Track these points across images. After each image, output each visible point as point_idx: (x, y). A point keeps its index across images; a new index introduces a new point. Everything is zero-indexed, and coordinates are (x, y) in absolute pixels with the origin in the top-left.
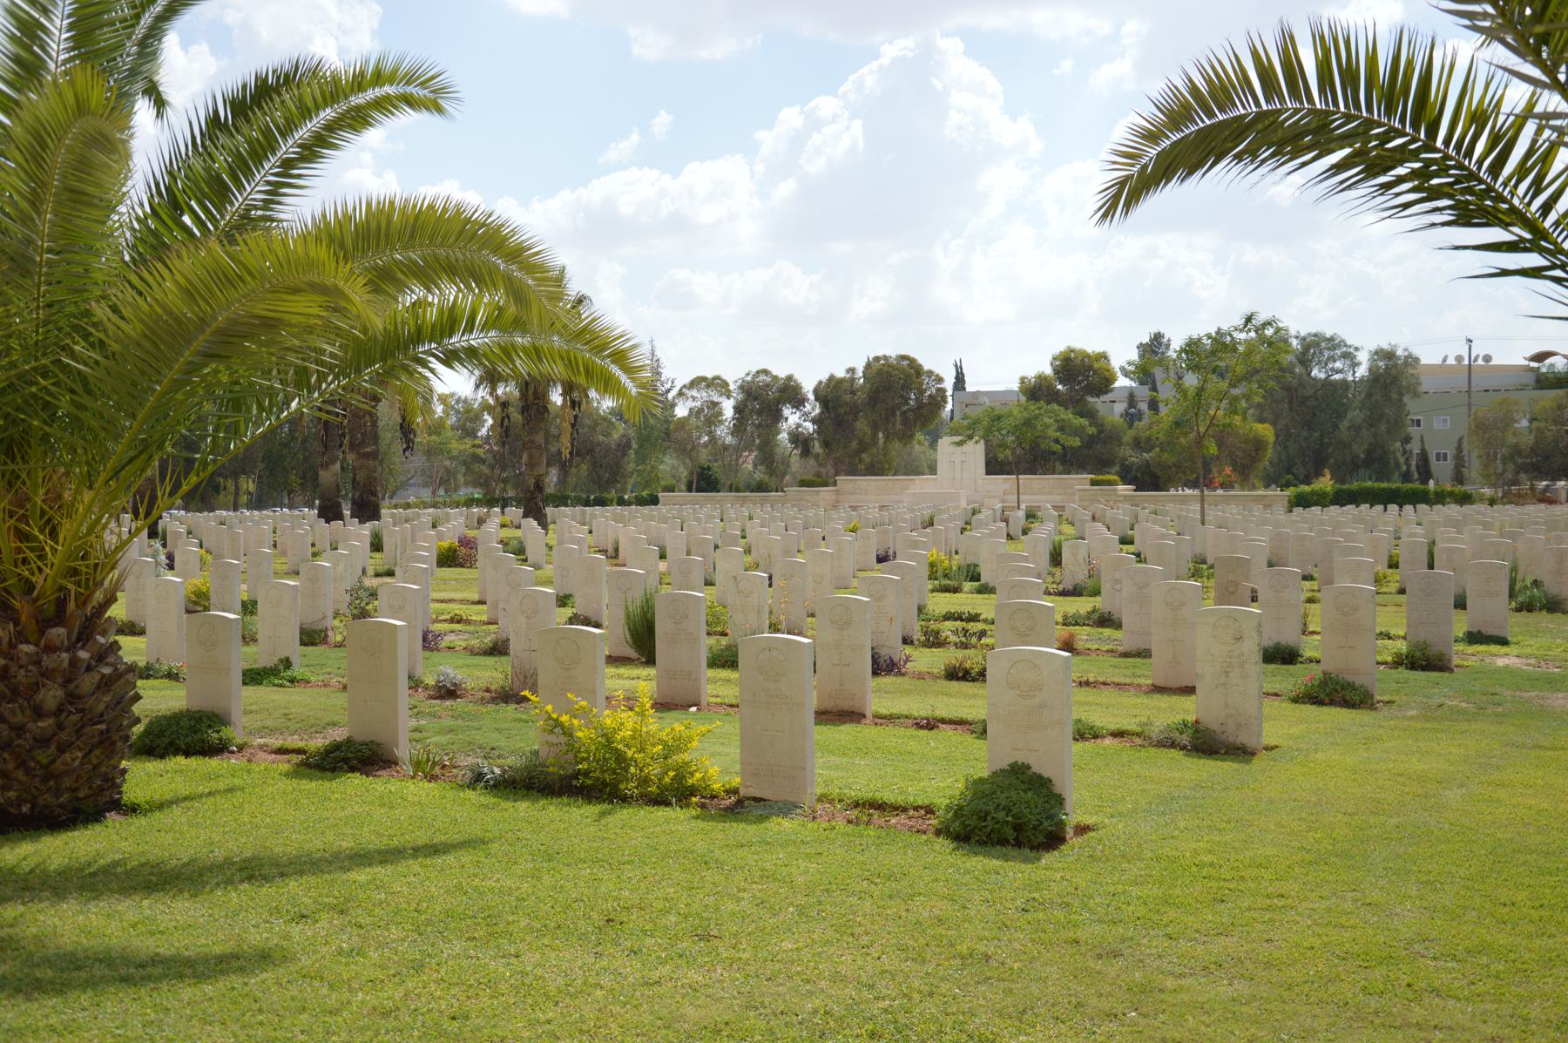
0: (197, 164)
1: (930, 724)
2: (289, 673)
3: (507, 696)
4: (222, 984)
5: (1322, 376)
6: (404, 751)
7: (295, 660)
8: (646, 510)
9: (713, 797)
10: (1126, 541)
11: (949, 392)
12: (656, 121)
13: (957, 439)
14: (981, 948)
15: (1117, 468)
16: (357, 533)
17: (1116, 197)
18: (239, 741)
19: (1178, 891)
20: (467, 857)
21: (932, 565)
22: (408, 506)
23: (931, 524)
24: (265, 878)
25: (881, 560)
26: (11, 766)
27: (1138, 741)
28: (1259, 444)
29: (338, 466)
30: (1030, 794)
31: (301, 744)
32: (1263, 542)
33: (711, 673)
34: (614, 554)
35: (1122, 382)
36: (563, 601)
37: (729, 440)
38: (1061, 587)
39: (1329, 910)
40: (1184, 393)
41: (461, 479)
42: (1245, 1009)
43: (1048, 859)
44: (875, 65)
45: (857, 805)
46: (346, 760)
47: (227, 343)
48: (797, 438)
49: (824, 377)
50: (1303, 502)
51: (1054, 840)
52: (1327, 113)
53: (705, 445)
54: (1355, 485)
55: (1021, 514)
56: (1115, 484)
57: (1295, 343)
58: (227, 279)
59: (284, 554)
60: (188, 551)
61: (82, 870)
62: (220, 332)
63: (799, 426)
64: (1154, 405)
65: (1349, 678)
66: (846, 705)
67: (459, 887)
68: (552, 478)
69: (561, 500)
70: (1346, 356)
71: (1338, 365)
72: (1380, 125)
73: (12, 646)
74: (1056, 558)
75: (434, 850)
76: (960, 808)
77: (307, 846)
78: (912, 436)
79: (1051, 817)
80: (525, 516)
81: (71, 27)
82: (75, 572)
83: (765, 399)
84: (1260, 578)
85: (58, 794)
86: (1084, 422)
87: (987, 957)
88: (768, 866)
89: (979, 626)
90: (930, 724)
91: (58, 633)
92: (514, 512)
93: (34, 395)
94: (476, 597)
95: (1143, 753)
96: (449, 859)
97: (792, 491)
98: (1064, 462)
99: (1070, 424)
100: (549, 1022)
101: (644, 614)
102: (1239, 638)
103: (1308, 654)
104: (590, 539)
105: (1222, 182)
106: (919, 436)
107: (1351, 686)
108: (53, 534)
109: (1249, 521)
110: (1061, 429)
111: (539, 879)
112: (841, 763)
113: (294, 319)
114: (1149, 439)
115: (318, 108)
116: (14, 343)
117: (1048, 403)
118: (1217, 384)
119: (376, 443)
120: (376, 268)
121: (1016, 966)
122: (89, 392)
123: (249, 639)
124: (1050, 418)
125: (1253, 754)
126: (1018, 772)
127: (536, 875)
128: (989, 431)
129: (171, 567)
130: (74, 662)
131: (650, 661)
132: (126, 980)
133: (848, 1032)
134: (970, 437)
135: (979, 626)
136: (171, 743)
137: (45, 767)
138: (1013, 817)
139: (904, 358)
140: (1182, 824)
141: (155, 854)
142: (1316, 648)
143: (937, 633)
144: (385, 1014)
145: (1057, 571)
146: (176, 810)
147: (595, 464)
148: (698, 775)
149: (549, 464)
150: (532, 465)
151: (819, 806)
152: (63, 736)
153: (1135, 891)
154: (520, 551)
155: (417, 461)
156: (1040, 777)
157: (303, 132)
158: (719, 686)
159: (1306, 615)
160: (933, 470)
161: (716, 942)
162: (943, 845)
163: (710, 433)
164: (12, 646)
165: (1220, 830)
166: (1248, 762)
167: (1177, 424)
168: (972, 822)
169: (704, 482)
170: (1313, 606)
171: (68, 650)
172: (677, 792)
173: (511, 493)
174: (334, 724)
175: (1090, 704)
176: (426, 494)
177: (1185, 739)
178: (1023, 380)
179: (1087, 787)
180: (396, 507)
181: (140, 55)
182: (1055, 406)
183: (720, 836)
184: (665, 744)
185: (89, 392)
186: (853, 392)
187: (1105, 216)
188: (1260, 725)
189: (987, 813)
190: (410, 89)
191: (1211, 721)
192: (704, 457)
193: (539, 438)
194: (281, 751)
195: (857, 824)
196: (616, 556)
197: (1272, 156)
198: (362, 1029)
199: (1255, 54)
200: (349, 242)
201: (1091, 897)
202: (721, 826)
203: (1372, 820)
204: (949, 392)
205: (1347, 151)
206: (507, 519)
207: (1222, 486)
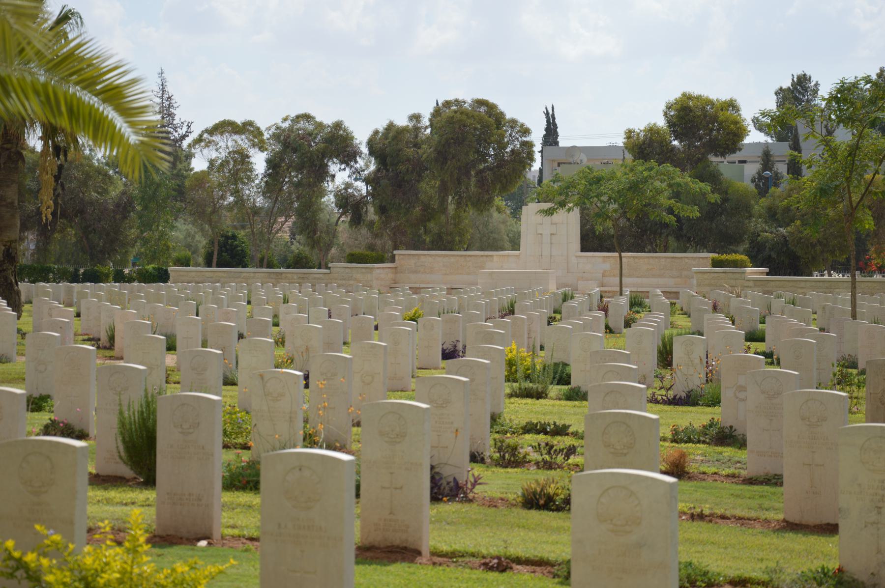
1: (502, 565)
10: (754, 337)
11: (538, 147)
13: (546, 206)
21: (511, 363)
23: (512, 312)
25: (449, 354)
33: (228, 497)
34: (107, 344)
35: (754, 137)
36: (36, 404)
37: (260, 201)
38: (671, 394)
40: (834, 152)
48: (345, 200)
49: (381, 126)
53: (230, 208)
55: (624, 301)
56: (742, 265)
63: (348, 186)
64: (795, 168)
66: (397, 539)
69: (39, 274)
74: (665, 357)
78: (490, 201)
83: (307, 150)
86: (706, 187)
89: (568, 441)
90: (502, 565)
97: (340, 267)
98: (678, 238)
106: (498, 201)
110: (677, 195)
114: (787, 209)
131: (150, 482)
134: (562, 204)
135: (568, 441)
139: (481, 103)
143: (514, 449)
149: (24, 227)
156: (725, 102)
158: (237, 514)
160: (515, 244)
163: (236, 192)
167: (823, 191)
169: (228, 254)
178: (629, 134)
182: (668, 167)
186: (417, 145)
192: (228, 222)
196: (111, 345)
204: (538, 147)
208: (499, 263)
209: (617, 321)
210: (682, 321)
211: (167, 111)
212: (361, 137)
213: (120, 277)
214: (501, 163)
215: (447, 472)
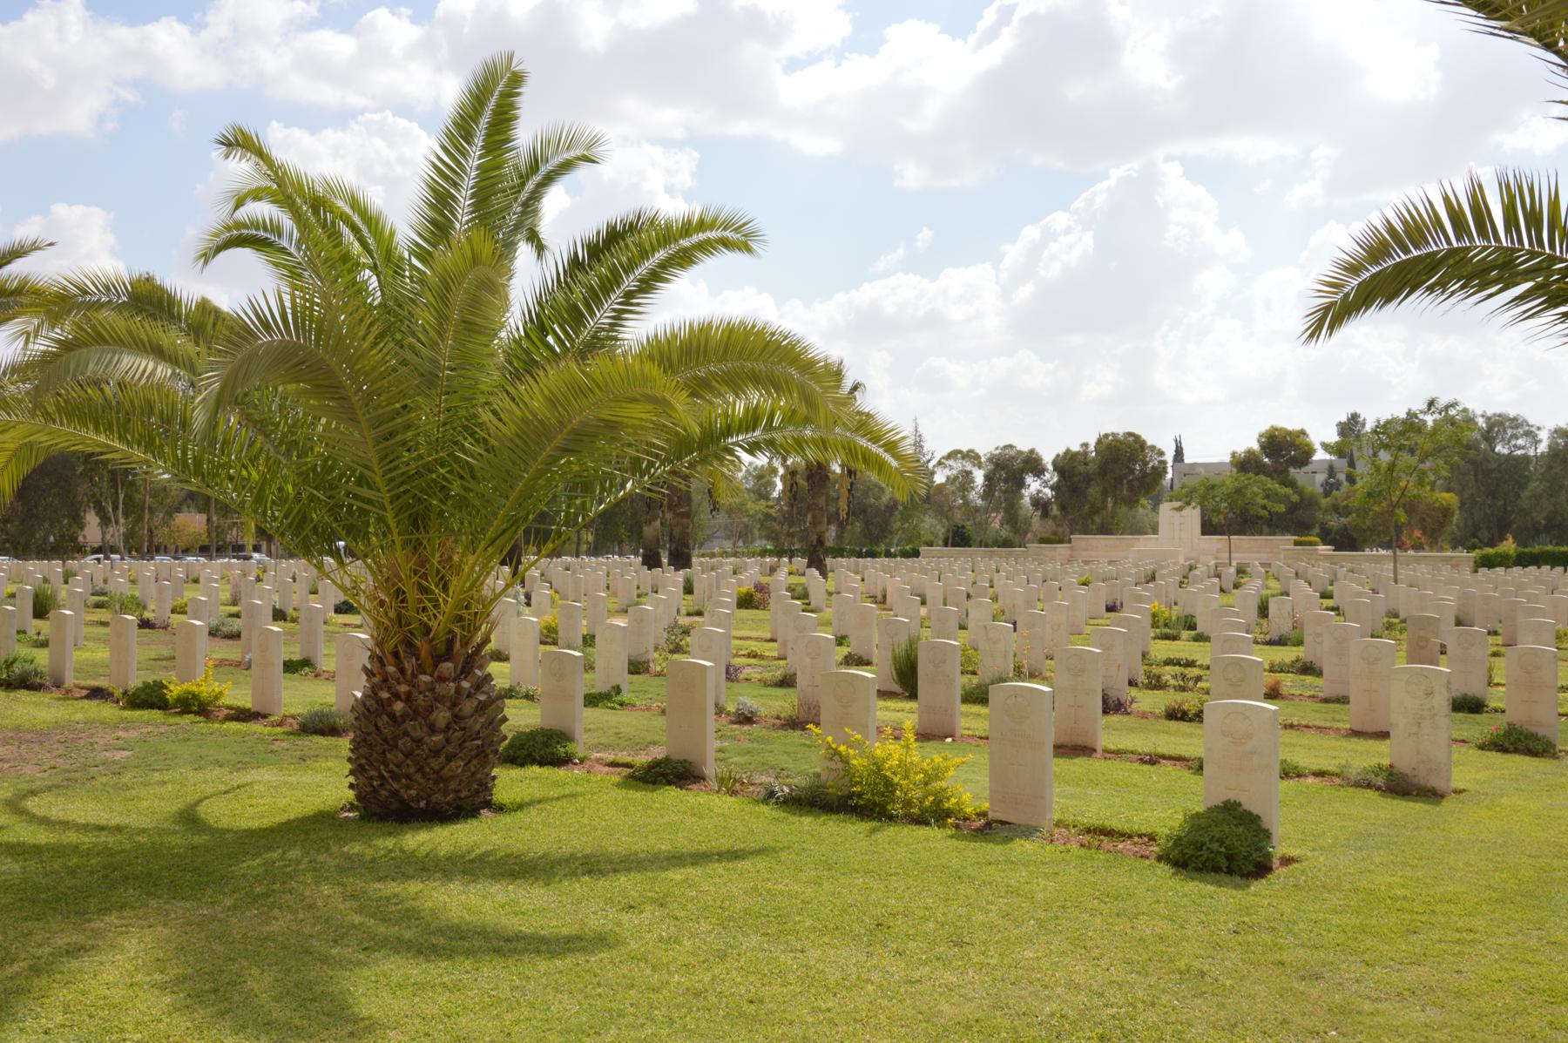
0: (560, 297)
1: (1153, 760)
2: (619, 698)
3: (793, 724)
4: (570, 960)
5: (1506, 451)
6: (710, 769)
7: (624, 687)
8: (909, 562)
9: (966, 819)
10: (1326, 595)
11: (1170, 464)
12: (920, 236)
13: (1178, 504)
14: (1197, 964)
15: (1317, 530)
16: (673, 578)
17: (1321, 322)
18: (581, 755)
19: (1374, 921)
20: (761, 863)
21: (1154, 616)
22: (713, 555)
23: (1153, 578)
24: (602, 873)
25: (1111, 609)
26: (412, 770)
27: (1337, 781)
28: (1446, 512)
29: (658, 523)
30: (1241, 829)
31: (629, 760)
32: (1451, 601)
33: (965, 708)
34: (881, 600)
35: (1320, 455)
36: (840, 641)
37: (979, 502)
38: (1268, 638)
39: (1515, 946)
40: (1378, 469)
41: (756, 533)
42: (1437, 1035)
43: (1257, 886)
44: (1105, 184)
45: (1089, 831)
46: (664, 775)
47: (580, 440)
48: (1037, 502)
49: (1061, 451)
50: (1488, 563)
51: (1261, 869)
52: (1513, 250)
53: (960, 507)
54: (1537, 549)
55: (1232, 570)
56: (1315, 544)
57: (1481, 422)
58: (581, 391)
59: (615, 594)
60: (542, 592)
61: (463, 856)
62: (573, 432)
63: (1039, 492)
64: (1351, 479)
65: (1533, 729)
66: (1080, 741)
67: (755, 889)
68: (831, 533)
69: (839, 552)
70: (1528, 434)
71: (1520, 442)
72: (1562, 260)
73: (414, 676)
74: (1263, 611)
75: (734, 855)
76: (1180, 838)
77: (634, 848)
78: (1137, 501)
79: (1259, 849)
80: (809, 566)
81: (473, 196)
82: (460, 619)
83: (1011, 469)
84: (1449, 634)
85: (446, 793)
86: (1288, 491)
87: (1202, 974)
88: (1013, 883)
89: (1196, 672)
90: (1153, 760)
91: (447, 667)
92: (800, 562)
93: (434, 481)
94: (768, 636)
95: (1342, 792)
96: (745, 864)
97: (1033, 547)
98: (1269, 526)
99: (1271, 492)
100: (829, 1010)
101: (908, 656)
102: (1430, 694)
103: (1493, 704)
104: (862, 587)
105: (1417, 306)
106: (1143, 501)
107: (1535, 737)
108: (445, 588)
109: (1439, 580)
110: (1267, 497)
111: (820, 885)
112: (1077, 793)
113: (631, 422)
114: (1346, 507)
115: (654, 250)
116: (421, 440)
117: (1256, 474)
118: (1406, 459)
119: (689, 505)
120: (696, 378)
121: (1228, 983)
122: (474, 477)
123: (590, 667)
124: (1258, 488)
125: (1442, 796)
126: (1231, 810)
127: (817, 882)
128: (1204, 498)
129: (528, 604)
130: (458, 690)
131: (913, 696)
132: (497, 951)
133: (1080, 1034)
134: (1188, 504)
135: (1196, 672)
136: (529, 755)
137: (437, 772)
138: (1225, 848)
139: (1130, 434)
140: (1377, 860)
141: (517, 847)
142: (1501, 699)
143: (1158, 677)
144: (697, 995)
145: (1264, 622)
146: (533, 811)
147: (867, 523)
148: (953, 800)
149: (829, 522)
150: (815, 524)
151: (1056, 830)
152: (450, 749)
153: (1336, 919)
154: (804, 596)
155: (722, 518)
156: (1250, 813)
157: (642, 270)
158: (972, 720)
159: (1490, 669)
160: (1155, 531)
161: (968, 948)
162: (1164, 870)
163: (963, 497)
164: (414, 676)
165: (1413, 867)
166: (1438, 803)
167: (1370, 495)
168: (1190, 851)
169: (959, 538)
170: (1497, 659)
171: (454, 680)
172: (936, 814)
173: (797, 546)
174: (655, 743)
175: (1294, 746)
176: (728, 546)
177: (1380, 781)
178: (1233, 454)
179: (1291, 823)
180: (703, 556)
181: (523, 213)
182: (1262, 477)
183: (972, 854)
184: (925, 772)
185: (474, 477)
186: (1086, 464)
187: (1311, 336)
188: (1449, 771)
189: (1203, 844)
190: (727, 234)
191: (1404, 766)
192: (958, 517)
193: (821, 502)
194: (614, 764)
195: (1089, 848)
196: (884, 601)
197: (1462, 288)
198: (678, 1006)
199: (1446, 200)
200: (675, 357)
201: (1295, 923)
202: (972, 845)
203: (1556, 864)
204: (1170, 464)
205: (1531, 284)
206: (794, 568)
207: (1413, 547)
208: (1144, 544)
209: (1228, 585)
210: (1273, 583)
211: (918, 444)
212: (1048, 459)
213: (888, 554)
214: (1144, 475)
215: (1113, 694)
